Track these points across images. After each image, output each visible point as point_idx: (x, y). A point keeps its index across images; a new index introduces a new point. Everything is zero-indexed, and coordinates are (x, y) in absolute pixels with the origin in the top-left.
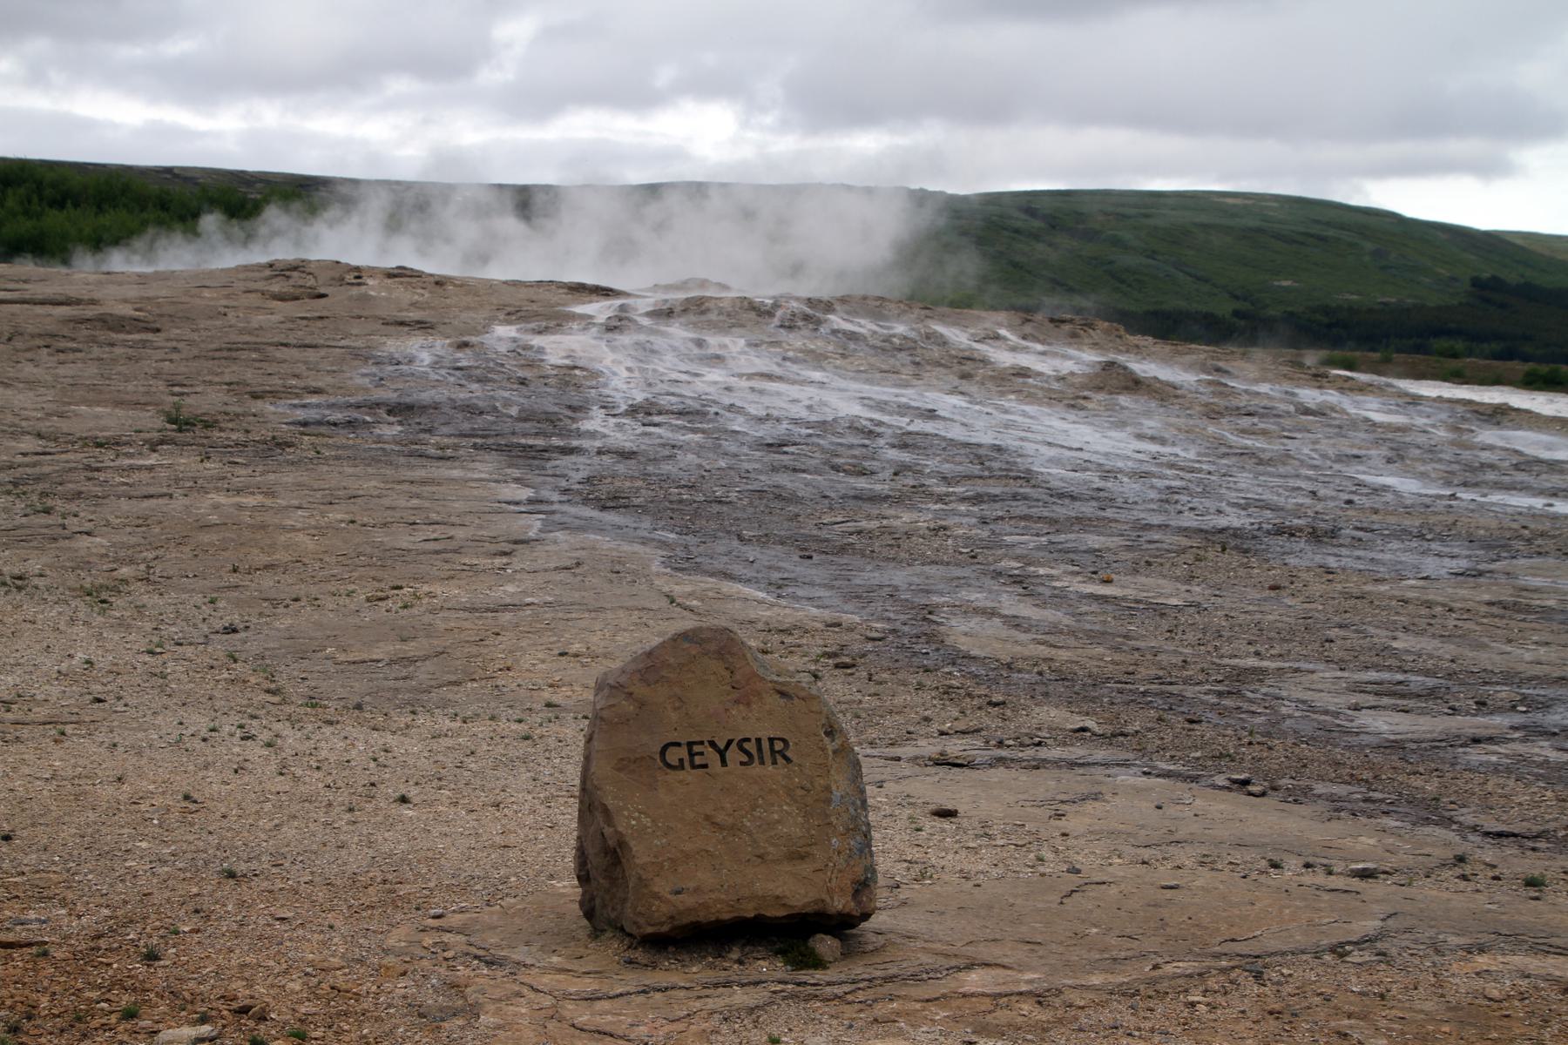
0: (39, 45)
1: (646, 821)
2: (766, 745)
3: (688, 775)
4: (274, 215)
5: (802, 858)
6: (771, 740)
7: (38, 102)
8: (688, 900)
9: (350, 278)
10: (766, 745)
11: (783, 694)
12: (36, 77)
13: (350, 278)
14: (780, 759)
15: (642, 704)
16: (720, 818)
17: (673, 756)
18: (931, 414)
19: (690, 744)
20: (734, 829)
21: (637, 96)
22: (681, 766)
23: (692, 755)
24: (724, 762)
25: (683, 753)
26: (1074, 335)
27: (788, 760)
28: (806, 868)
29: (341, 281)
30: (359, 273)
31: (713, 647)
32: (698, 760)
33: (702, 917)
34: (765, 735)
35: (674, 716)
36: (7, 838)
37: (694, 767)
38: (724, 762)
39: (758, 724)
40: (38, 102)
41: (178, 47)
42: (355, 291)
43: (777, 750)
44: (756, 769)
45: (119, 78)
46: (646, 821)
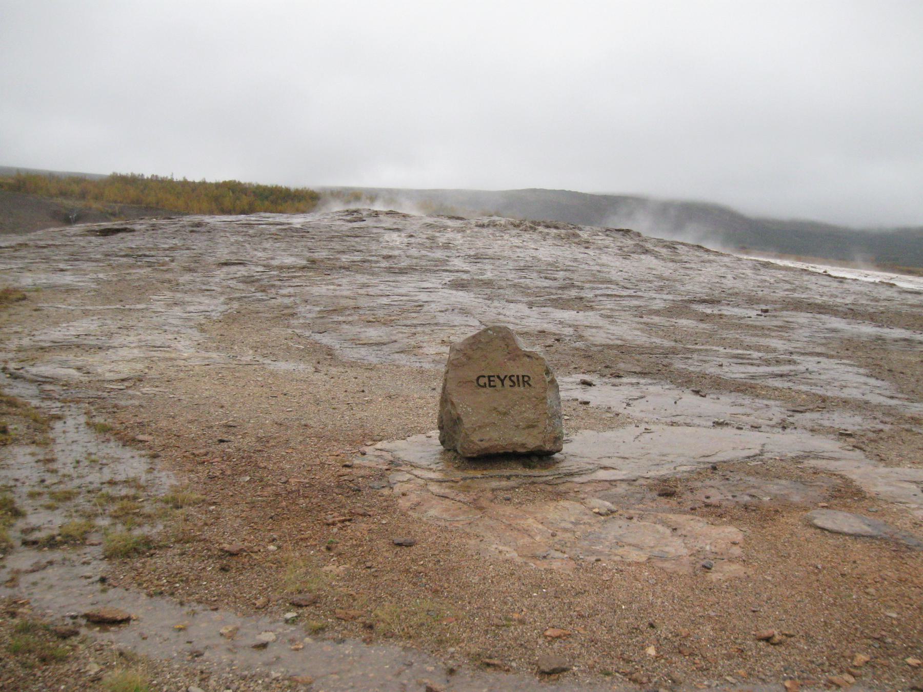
2: (521, 379)
6: (523, 376)
8: (485, 445)
10: (521, 379)
14: (527, 385)
15: (469, 358)
16: (501, 409)
17: (482, 381)
19: (489, 377)
22: (485, 386)
23: (490, 381)
25: (486, 380)
27: (530, 385)
34: (520, 373)
37: (490, 386)
38: (503, 385)
44: (516, 389)
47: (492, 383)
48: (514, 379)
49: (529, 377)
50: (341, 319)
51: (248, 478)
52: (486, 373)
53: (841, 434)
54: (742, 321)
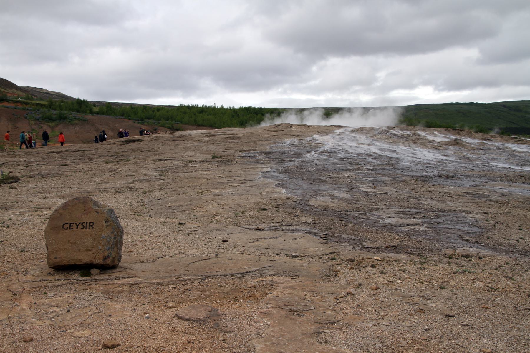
0: (286, 86)
1: (54, 241)
2: (88, 224)
3: (68, 231)
4: (283, 115)
5: (90, 251)
6: (90, 223)
7: (285, 97)
8: (57, 260)
9: (289, 127)
10: (88, 224)
11: (97, 212)
12: (285, 92)
13: (289, 127)
14: (91, 227)
15: (61, 214)
16: (72, 241)
17: (65, 227)
18: (394, 151)
19: (70, 224)
20: (74, 244)
21: (411, 86)
22: (67, 229)
23: (70, 226)
24: (77, 228)
25: (68, 226)
26: (458, 133)
27: (93, 228)
28: (90, 253)
29: (287, 127)
30: (291, 125)
31: (82, 201)
32: (71, 227)
33: (61, 264)
34: (88, 222)
35: (68, 217)
36: (2, 242)
37: (70, 229)
38: (77, 228)
39: (87, 219)
40: (285, 97)
41: (313, 83)
42: (289, 129)
43: (91, 225)
44: (84, 230)
45: (300, 91)
46: (54, 241)
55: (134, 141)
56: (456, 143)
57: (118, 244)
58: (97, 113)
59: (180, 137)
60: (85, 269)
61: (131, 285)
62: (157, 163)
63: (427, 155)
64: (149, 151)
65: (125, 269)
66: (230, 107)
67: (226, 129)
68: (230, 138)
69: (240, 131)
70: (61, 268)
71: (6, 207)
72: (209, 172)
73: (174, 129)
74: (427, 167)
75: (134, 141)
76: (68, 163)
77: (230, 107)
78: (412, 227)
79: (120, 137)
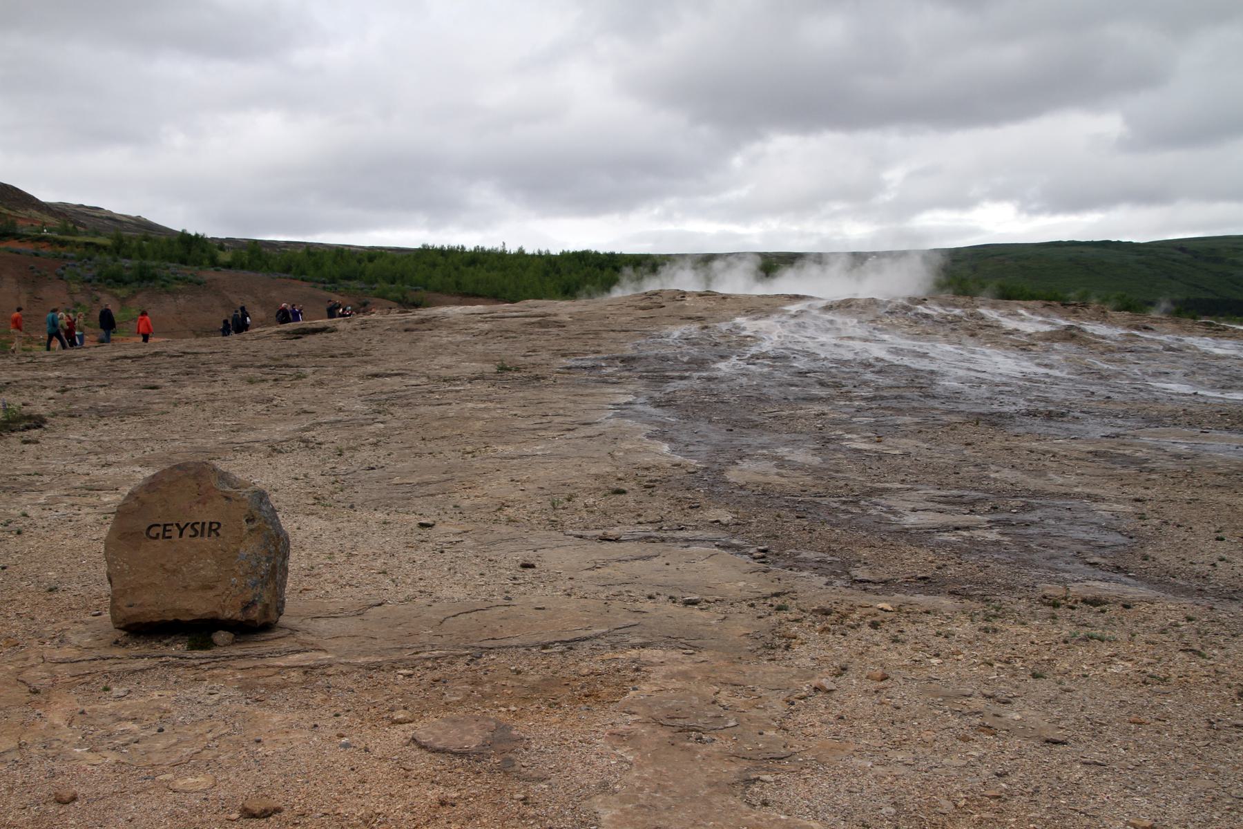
0: (672, 201)
1: (126, 567)
2: (207, 526)
3: (160, 542)
4: (664, 271)
5: (211, 588)
6: (211, 523)
7: (669, 227)
8: (135, 610)
9: (678, 297)
10: (207, 526)
11: (227, 498)
12: (668, 216)
13: (678, 297)
14: (213, 534)
15: (143, 503)
16: (168, 566)
17: (153, 533)
18: (924, 355)
19: (165, 525)
20: (174, 572)
21: (963, 202)
22: (157, 537)
23: (165, 530)
24: (181, 535)
25: (160, 530)
26: (1075, 312)
27: (218, 535)
28: (211, 594)
29: (674, 299)
30: (684, 295)
31: (192, 472)
32: (167, 534)
33: (142, 619)
34: (207, 520)
35: (160, 510)
37: (164, 537)
38: (181, 535)
39: (205, 515)
40: (669, 227)
41: (733, 195)
42: (679, 303)
43: (213, 529)
44: (198, 539)
45: (704, 213)
46: (126, 567)
47: (167, 534)
48: (198, 527)
49: (219, 524)
50: (510, 449)
51: (1018, 717)
52: (161, 522)
53: (1047, 741)
54: (548, 318)
55: (315, 331)
56: (1069, 335)
57: (276, 573)
58: (229, 266)
59: (422, 321)
60: (199, 632)
61: (307, 670)
62: (367, 383)
63: (1003, 364)
64: (350, 355)
65: (293, 631)
66: (540, 252)
67: (531, 302)
68: (540, 325)
69: (563, 308)
70: (143, 630)
71: (13, 487)
72: (491, 405)
73: (407, 304)
74: (1001, 393)
75: (315, 331)
76: (159, 382)
77: (540, 252)
78: (965, 533)
79: (282, 322)
